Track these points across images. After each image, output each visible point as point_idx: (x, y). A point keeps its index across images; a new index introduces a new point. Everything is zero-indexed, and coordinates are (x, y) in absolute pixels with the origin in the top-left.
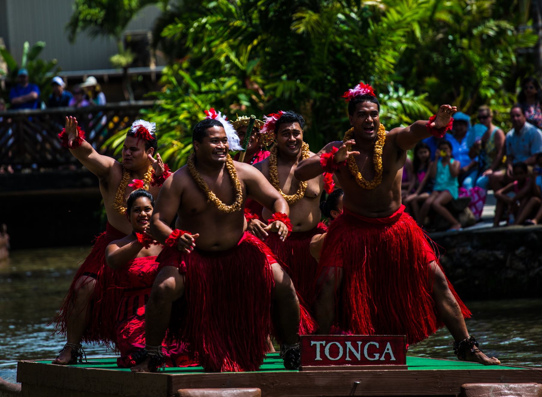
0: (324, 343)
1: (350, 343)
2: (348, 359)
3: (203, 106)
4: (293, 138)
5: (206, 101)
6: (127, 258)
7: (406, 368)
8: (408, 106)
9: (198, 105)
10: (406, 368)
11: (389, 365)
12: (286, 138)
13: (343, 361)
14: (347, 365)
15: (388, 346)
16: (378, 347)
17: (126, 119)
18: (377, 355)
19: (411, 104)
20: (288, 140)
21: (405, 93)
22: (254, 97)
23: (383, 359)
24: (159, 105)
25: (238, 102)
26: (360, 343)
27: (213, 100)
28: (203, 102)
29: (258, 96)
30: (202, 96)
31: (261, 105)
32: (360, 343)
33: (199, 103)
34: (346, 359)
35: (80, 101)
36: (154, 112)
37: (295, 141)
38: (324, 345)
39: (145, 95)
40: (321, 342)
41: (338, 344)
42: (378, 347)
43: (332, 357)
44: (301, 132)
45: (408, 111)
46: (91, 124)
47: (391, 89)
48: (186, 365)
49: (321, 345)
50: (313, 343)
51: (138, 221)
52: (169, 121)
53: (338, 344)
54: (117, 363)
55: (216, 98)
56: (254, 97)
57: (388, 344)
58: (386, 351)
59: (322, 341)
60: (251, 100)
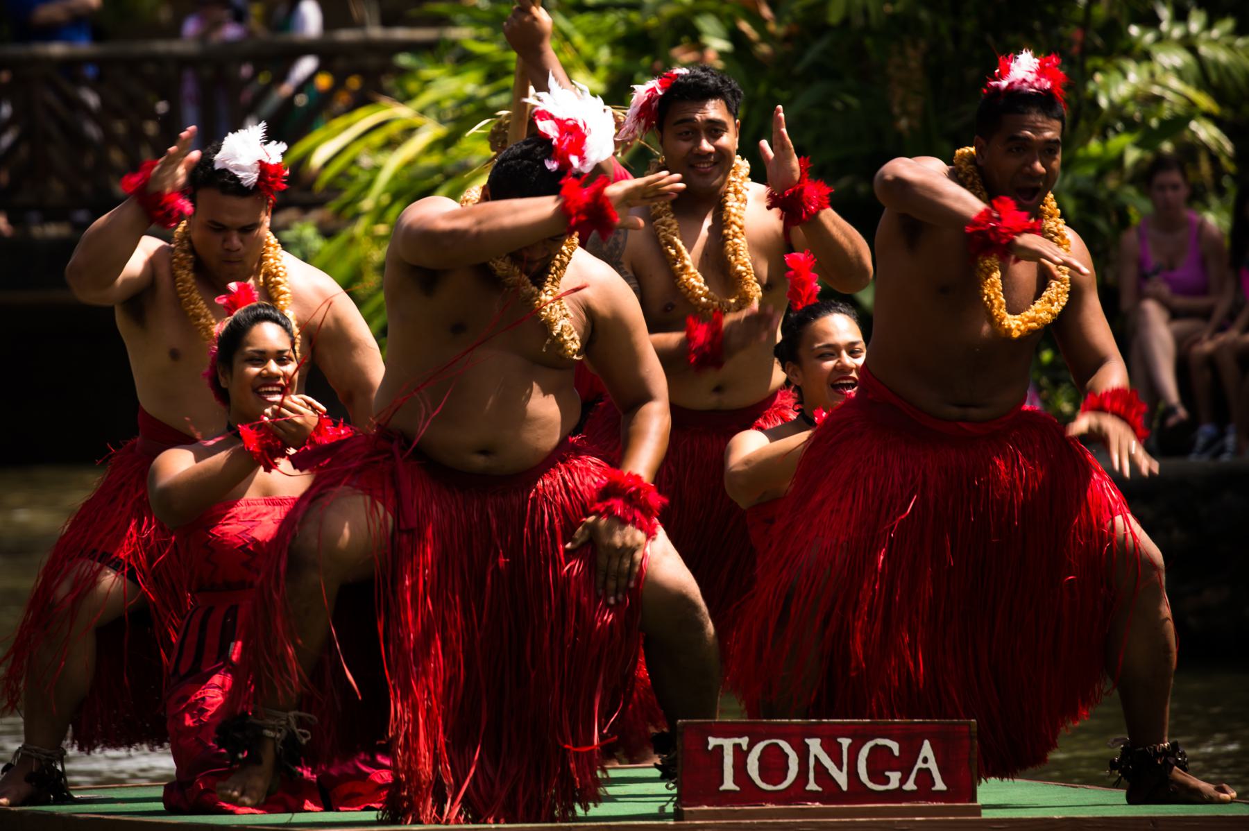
0: (744, 742)
1: (818, 741)
2: (812, 786)
3: (587, 49)
4: (706, 146)
5: (598, 34)
6: (216, 494)
7: (977, 810)
8: (1216, 64)
9: (572, 44)
10: (977, 810)
11: (930, 804)
12: (685, 146)
13: (798, 792)
14: (810, 805)
15: (927, 749)
16: (896, 753)
17: (354, 83)
18: (895, 777)
19: (1223, 56)
20: (691, 150)
21: (1209, 26)
22: (745, 26)
23: (910, 786)
24: (454, 44)
25: (696, 40)
26: (845, 742)
27: (621, 29)
28: (588, 37)
29: (758, 22)
30: (586, 20)
31: (764, 49)
32: (845, 742)
33: (578, 39)
34: (808, 788)
35: (217, 25)
36: (438, 62)
37: (710, 153)
38: (745, 747)
39: (414, 12)
40: (737, 740)
41: (784, 744)
42: (896, 753)
43: (768, 783)
44: (731, 127)
45: (1214, 76)
46: (247, 96)
47: (1165, 13)
48: (358, 805)
49: (737, 747)
50: (713, 742)
51: (256, 390)
52: (484, 91)
53: (784, 744)
54: (163, 799)
55: (629, 23)
56: (745, 26)
57: (927, 743)
58: (920, 764)
59: (740, 736)
60: (735, 36)
